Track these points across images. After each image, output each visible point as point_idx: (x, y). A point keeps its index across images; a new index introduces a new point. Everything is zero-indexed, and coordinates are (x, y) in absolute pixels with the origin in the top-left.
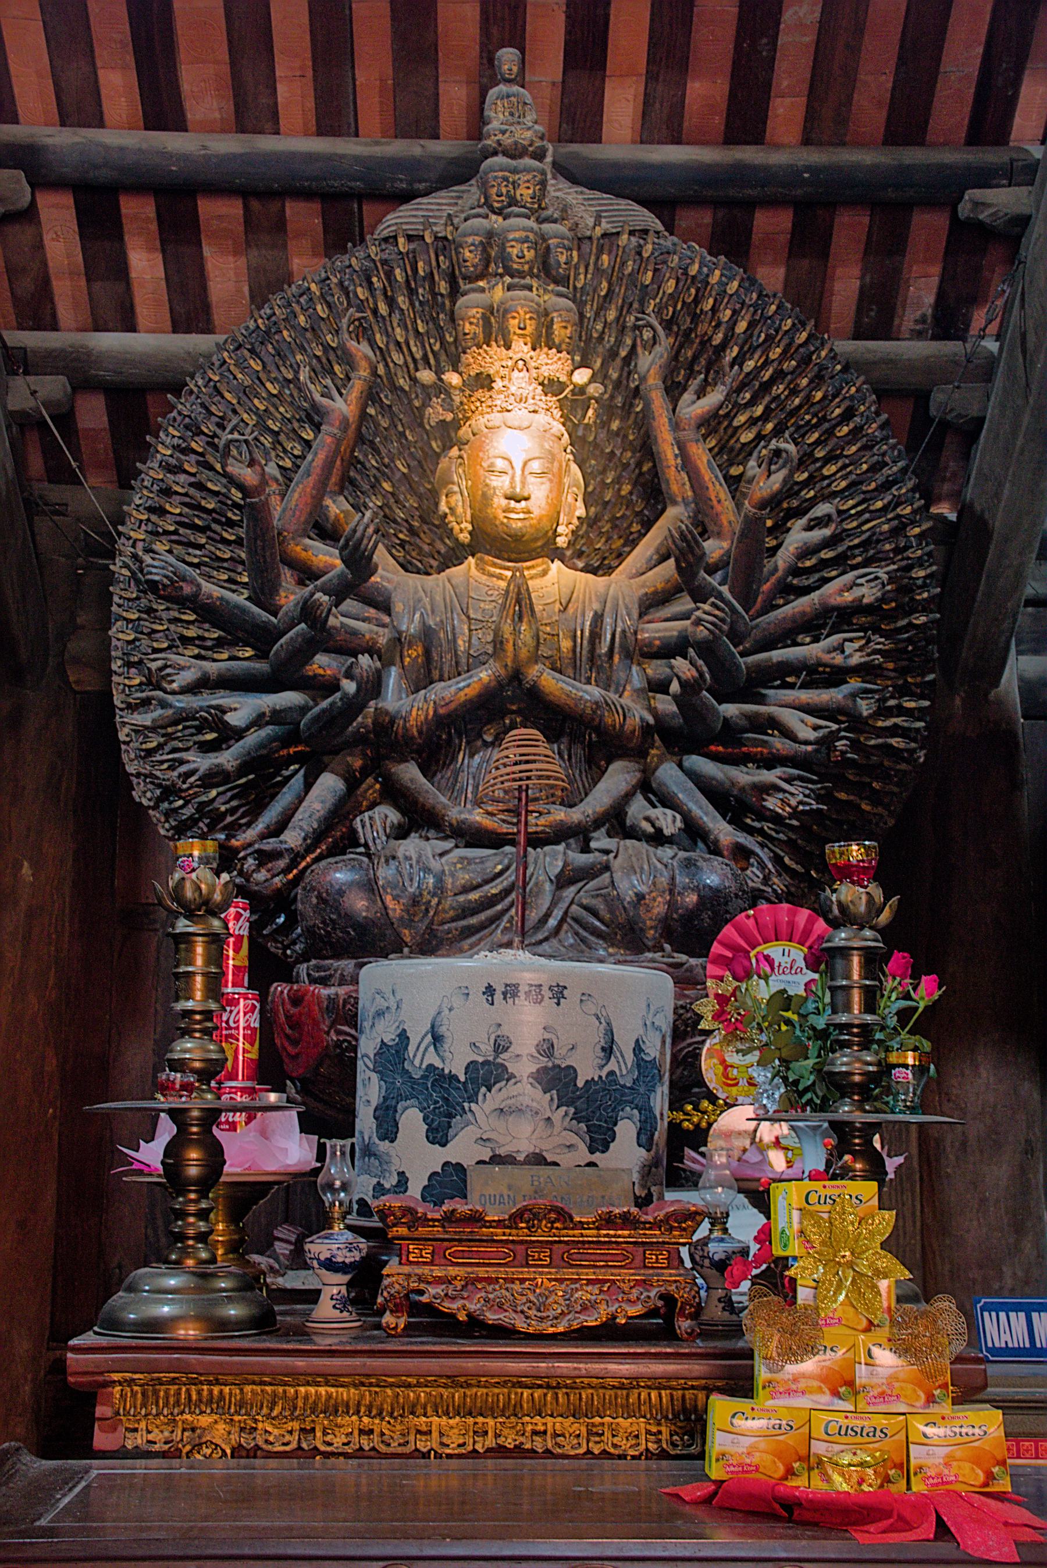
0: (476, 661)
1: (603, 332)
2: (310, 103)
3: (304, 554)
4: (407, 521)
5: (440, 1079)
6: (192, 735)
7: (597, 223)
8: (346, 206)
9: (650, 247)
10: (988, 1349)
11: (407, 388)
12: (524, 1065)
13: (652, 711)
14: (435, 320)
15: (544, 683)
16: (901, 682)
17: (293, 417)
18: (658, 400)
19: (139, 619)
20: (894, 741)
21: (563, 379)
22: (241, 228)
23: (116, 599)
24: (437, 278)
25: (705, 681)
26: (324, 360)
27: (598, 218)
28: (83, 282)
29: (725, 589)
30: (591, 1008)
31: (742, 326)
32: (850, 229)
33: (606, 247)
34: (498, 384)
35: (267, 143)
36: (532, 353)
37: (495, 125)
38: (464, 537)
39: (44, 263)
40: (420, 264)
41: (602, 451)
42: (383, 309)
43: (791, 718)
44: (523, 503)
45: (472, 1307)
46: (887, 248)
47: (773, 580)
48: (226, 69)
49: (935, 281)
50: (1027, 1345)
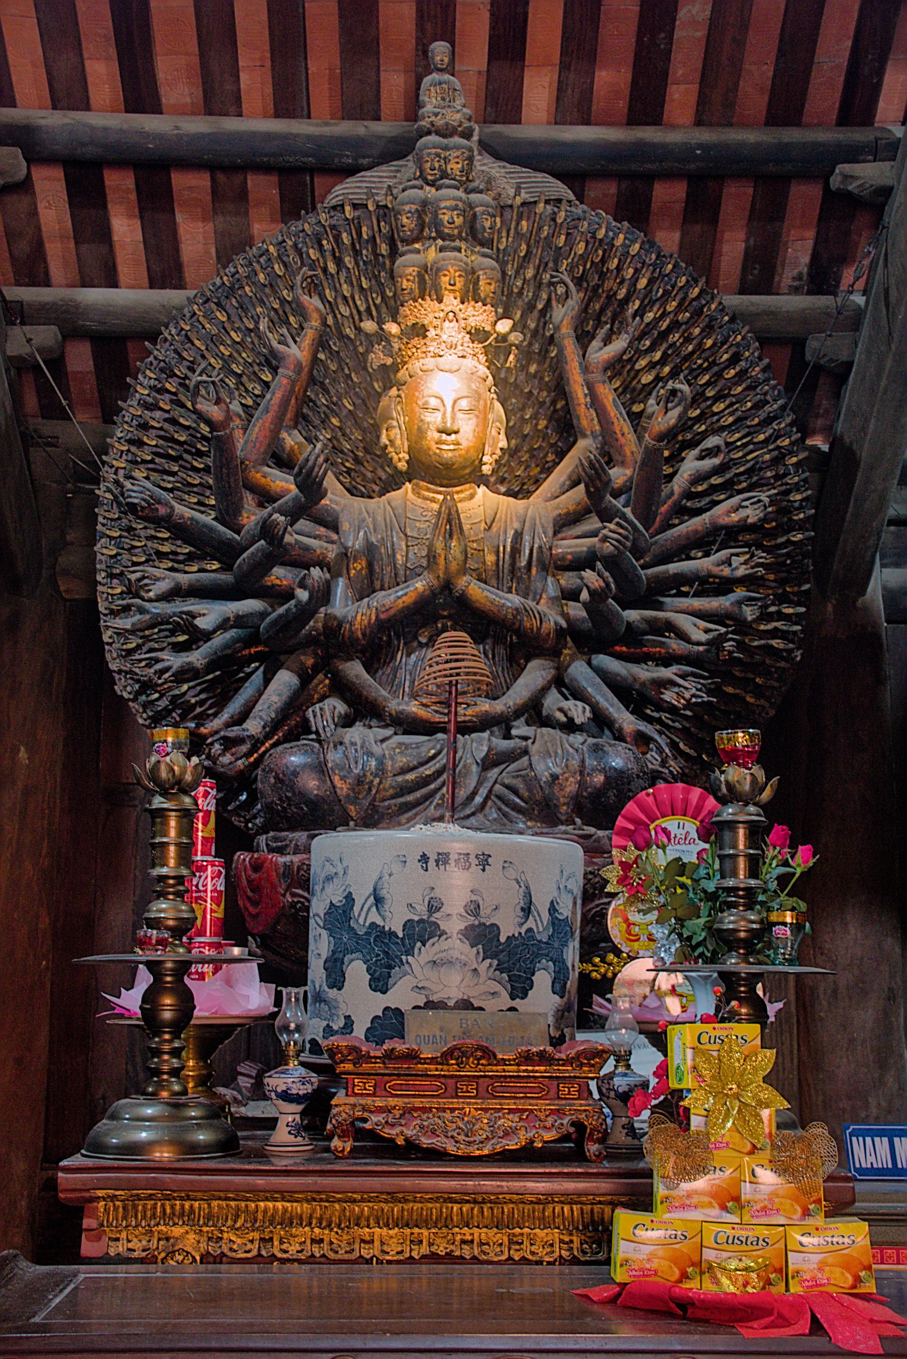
0: (413, 573)
1: (523, 288)
2: (269, 89)
3: (263, 480)
4: (352, 452)
5: (381, 935)
6: (166, 637)
7: (517, 193)
8: (300, 178)
9: (563, 214)
10: (856, 1169)
11: (352, 336)
12: (454, 923)
13: (565, 616)
14: (377, 277)
15: (471, 592)
16: (780, 591)
17: (254, 361)
18: (570, 347)
19: (120, 537)
20: (775, 643)
21: (488, 328)
22: (209, 198)
23: (100, 519)
24: (378, 241)
25: (611, 590)
26: (281, 312)
27: (518, 189)
28: (72, 245)
29: (628, 511)
30: (512, 873)
31: (643, 283)
32: (736, 198)
33: (525, 214)
34: (432, 333)
35: (231, 124)
36: (461, 306)
37: (429, 108)
38: (402, 466)
39: (39, 228)
40: (364, 229)
41: (522, 391)
42: (332, 267)
43: (685, 622)
44: (453, 436)
45: (409, 1133)
46: (768, 215)
47: (670, 502)
48: (196, 60)
49: (810, 243)
50: (890, 1166)
